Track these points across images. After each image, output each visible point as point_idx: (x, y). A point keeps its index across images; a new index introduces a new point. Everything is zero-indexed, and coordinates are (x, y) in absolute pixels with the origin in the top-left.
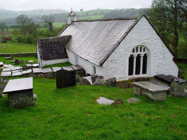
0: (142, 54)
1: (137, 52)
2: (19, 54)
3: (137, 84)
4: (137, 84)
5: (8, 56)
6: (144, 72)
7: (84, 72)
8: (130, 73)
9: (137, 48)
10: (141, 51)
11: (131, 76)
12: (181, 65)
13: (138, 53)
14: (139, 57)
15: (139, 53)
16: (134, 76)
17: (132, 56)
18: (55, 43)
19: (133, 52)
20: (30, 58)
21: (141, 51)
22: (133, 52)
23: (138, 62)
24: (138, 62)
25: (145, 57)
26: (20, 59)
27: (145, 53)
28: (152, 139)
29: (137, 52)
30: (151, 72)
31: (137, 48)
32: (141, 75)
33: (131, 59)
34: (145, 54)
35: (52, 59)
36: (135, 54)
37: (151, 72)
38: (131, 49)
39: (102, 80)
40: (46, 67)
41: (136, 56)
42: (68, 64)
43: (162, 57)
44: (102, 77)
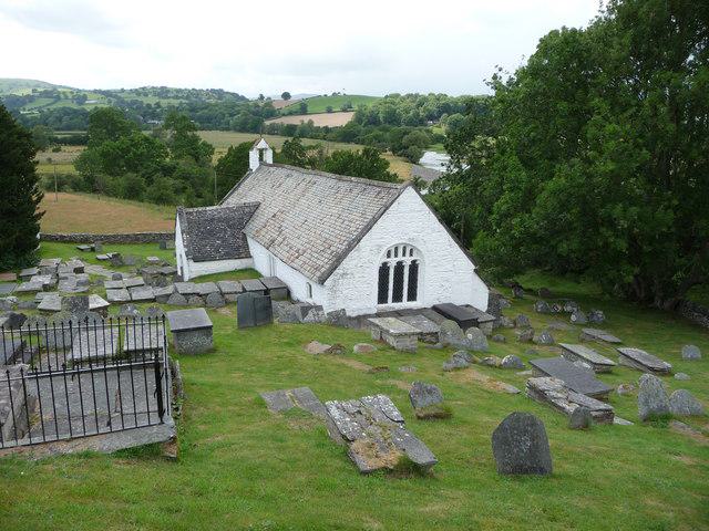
0: (407, 261)
1: (396, 256)
2: (114, 236)
3: (376, 321)
4: (376, 321)
5: (85, 240)
6: (412, 296)
7: (289, 293)
8: (382, 298)
9: (396, 249)
10: (404, 255)
11: (384, 305)
12: (497, 291)
13: (398, 259)
14: (400, 267)
15: (400, 258)
16: (391, 305)
17: (385, 264)
18: (219, 220)
19: (389, 256)
20: (149, 247)
21: (404, 255)
22: (389, 256)
23: (398, 279)
24: (398, 279)
25: (414, 267)
26: (126, 251)
27: (413, 258)
28: (459, 526)
29: (396, 256)
30: (428, 296)
31: (396, 249)
32: (405, 304)
33: (384, 270)
34: (414, 262)
35: (214, 259)
36: (393, 262)
37: (428, 296)
38: (384, 251)
39: (320, 313)
40: (201, 279)
41: (394, 264)
42: (252, 272)
43: (449, 267)
44: (319, 308)
